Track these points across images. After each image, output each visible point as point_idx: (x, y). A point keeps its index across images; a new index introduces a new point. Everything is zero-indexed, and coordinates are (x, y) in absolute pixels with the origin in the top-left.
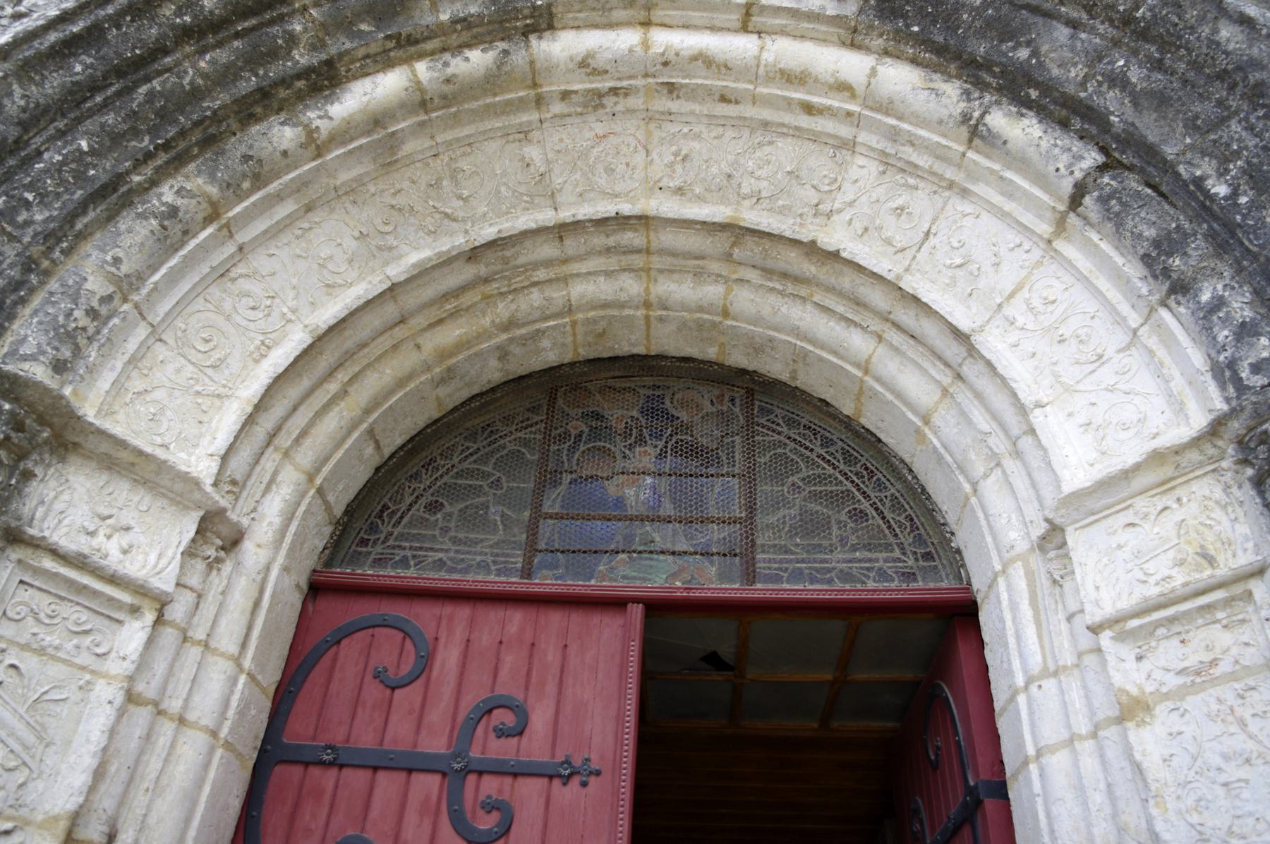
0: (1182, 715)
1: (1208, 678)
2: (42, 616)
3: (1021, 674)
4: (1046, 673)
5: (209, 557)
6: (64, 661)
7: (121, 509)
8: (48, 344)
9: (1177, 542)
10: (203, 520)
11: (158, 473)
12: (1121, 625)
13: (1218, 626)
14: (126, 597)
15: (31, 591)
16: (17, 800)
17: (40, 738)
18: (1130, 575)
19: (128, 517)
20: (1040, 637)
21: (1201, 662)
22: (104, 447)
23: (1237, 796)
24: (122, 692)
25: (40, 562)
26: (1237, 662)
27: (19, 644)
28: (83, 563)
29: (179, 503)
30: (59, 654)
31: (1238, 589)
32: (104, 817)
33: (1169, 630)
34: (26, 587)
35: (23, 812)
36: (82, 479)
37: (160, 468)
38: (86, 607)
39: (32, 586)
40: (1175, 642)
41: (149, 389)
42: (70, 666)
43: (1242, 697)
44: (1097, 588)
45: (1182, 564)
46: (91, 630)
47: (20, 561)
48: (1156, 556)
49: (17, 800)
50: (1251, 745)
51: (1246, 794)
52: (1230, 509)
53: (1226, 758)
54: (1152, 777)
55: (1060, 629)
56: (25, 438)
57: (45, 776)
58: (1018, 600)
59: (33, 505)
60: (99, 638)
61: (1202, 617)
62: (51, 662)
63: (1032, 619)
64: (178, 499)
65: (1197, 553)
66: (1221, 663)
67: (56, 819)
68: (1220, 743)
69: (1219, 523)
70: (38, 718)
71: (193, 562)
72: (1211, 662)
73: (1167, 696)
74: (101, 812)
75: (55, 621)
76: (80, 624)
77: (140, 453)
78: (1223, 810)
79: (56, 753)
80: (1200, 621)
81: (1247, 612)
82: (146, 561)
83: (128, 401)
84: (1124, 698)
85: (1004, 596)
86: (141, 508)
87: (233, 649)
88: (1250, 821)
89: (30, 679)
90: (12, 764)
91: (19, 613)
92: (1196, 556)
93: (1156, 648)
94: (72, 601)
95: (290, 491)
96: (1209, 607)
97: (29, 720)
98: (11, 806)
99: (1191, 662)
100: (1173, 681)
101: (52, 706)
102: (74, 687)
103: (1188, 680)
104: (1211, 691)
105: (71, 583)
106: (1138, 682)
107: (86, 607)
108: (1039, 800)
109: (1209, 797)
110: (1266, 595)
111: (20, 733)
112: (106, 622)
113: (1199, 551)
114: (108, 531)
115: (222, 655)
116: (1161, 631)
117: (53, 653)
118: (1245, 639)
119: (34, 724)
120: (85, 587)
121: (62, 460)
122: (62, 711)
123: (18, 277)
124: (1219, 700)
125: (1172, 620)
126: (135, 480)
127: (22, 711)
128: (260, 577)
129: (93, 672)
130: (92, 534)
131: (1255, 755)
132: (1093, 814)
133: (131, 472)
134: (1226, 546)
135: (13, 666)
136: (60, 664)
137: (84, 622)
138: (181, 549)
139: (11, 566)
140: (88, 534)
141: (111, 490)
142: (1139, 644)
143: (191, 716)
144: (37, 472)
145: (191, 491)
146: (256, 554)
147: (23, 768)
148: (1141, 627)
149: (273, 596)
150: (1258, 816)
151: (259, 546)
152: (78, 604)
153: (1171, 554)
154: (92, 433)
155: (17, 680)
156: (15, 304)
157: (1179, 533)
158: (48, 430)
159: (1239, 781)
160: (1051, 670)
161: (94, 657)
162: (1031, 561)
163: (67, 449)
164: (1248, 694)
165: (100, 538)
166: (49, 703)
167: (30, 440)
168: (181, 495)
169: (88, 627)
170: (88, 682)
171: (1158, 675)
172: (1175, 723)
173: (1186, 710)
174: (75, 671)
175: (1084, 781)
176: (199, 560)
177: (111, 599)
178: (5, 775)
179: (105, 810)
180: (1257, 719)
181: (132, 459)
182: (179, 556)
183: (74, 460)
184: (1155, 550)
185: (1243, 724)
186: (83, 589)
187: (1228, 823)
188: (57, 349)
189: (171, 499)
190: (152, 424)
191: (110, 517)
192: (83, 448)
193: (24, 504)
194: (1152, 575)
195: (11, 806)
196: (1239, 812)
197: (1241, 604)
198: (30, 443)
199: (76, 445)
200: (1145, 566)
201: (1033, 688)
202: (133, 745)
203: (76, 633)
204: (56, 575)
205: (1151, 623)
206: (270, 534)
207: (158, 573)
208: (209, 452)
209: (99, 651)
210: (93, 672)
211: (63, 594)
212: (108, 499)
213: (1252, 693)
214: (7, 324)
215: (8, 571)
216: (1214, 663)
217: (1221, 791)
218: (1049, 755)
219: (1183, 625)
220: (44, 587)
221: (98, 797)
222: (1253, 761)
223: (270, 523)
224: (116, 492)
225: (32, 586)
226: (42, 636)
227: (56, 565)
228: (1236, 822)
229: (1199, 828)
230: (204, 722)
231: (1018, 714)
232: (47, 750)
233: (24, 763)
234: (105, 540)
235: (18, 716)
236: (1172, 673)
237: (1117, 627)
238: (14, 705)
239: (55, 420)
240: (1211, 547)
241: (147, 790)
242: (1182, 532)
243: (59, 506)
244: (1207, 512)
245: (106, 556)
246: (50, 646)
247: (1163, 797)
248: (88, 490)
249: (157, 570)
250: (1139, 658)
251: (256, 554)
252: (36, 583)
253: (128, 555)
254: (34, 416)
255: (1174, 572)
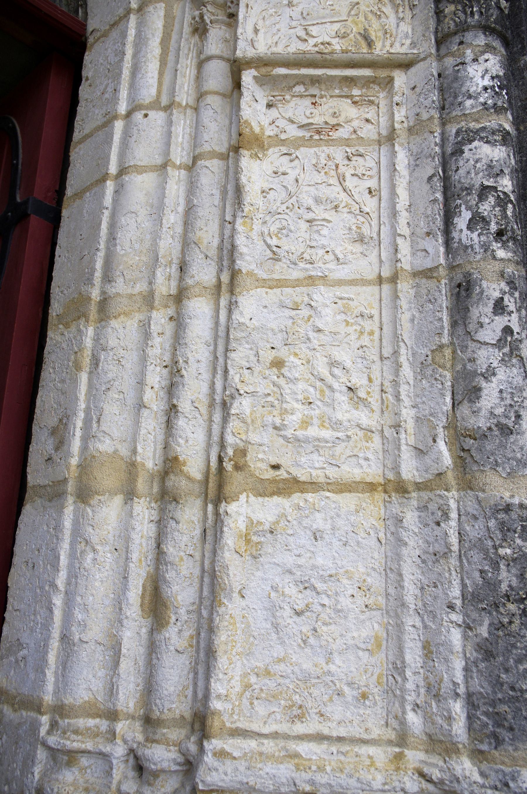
0: (291, 161)
1: (326, 138)
3: (125, 104)
4: (156, 105)
9: (345, 18)
12: (269, 69)
13: (349, 101)
18: (292, 31)
20: (161, 74)
21: (326, 123)
23: (318, 232)
26: (355, 132)
31: (383, 73)
33: (306, 90)
40: (307, 102)
43: (349, 159)
44: (256, 31)
45: (344, 37)
48: (322, 23)
50: (343, 196)
51: (325, 231)
52: (401, 9)
53: (318, 201)
54: (249, 201)
55: (185, 73)
58: (150, 36)
61: (341, 89)
63: (158, 57)
65: (360, 33)
66: (341, 130)
68: (317, 189)
69: (387, 17)
72: (334, 126)
73: (283, 142)
78: (301, 240)
80: (337, 91)
81: (378, 97)
84: (247, 130)
85: (132, 32)
88: (321, 252)
92: (358, 37)
93: (289, 102)
96: (350, 81)
99: (318, 120)
100: (293, 132)
103: (308, 135)
104: (325, 148)
106: (262, 124)
108: (106, 213)
109: (292, 228)
110: (404, 86)
113: (362, 32)
116: (299, 89)
118: (368, 116)
124: (328, 156)
125: (315, 81)
131: (343, 204)
132: (164, 229)
134: (388, 36)
142: (274, 94)
148: (286, 76)
150: (327, 249)
153: (336, 26)
157: (350, 12)
159: (324, 220)
160: (162, 105)
162: (175, 7)
164: (354, 158)
171: (282, 123)
172: (284, 164)
173: (297, 157)
175: (166, 200)
180: (356, 178)
184: (324, 18)
185: (342, 179)
187: (302, 250)
194: (314, 37)
196: (313, 244)
197: (377, 88)
200: (310, 28)
201: (138, 116)
205: (296, 76)
213: (360, 159)
216: (335, 127)
217: (304, 226)
218: (135, 174)
219: (321, 90)
222: (340, 209)
228: (309, 250)
229: (275, 249)
231: (112, 135)
236: (295, 126)
237: (264, 70)
240: (373, 34)
242: (353, 13)
244: (380, 6)
247: (252, 219)
250: (269, 106)
255: (334, 41)
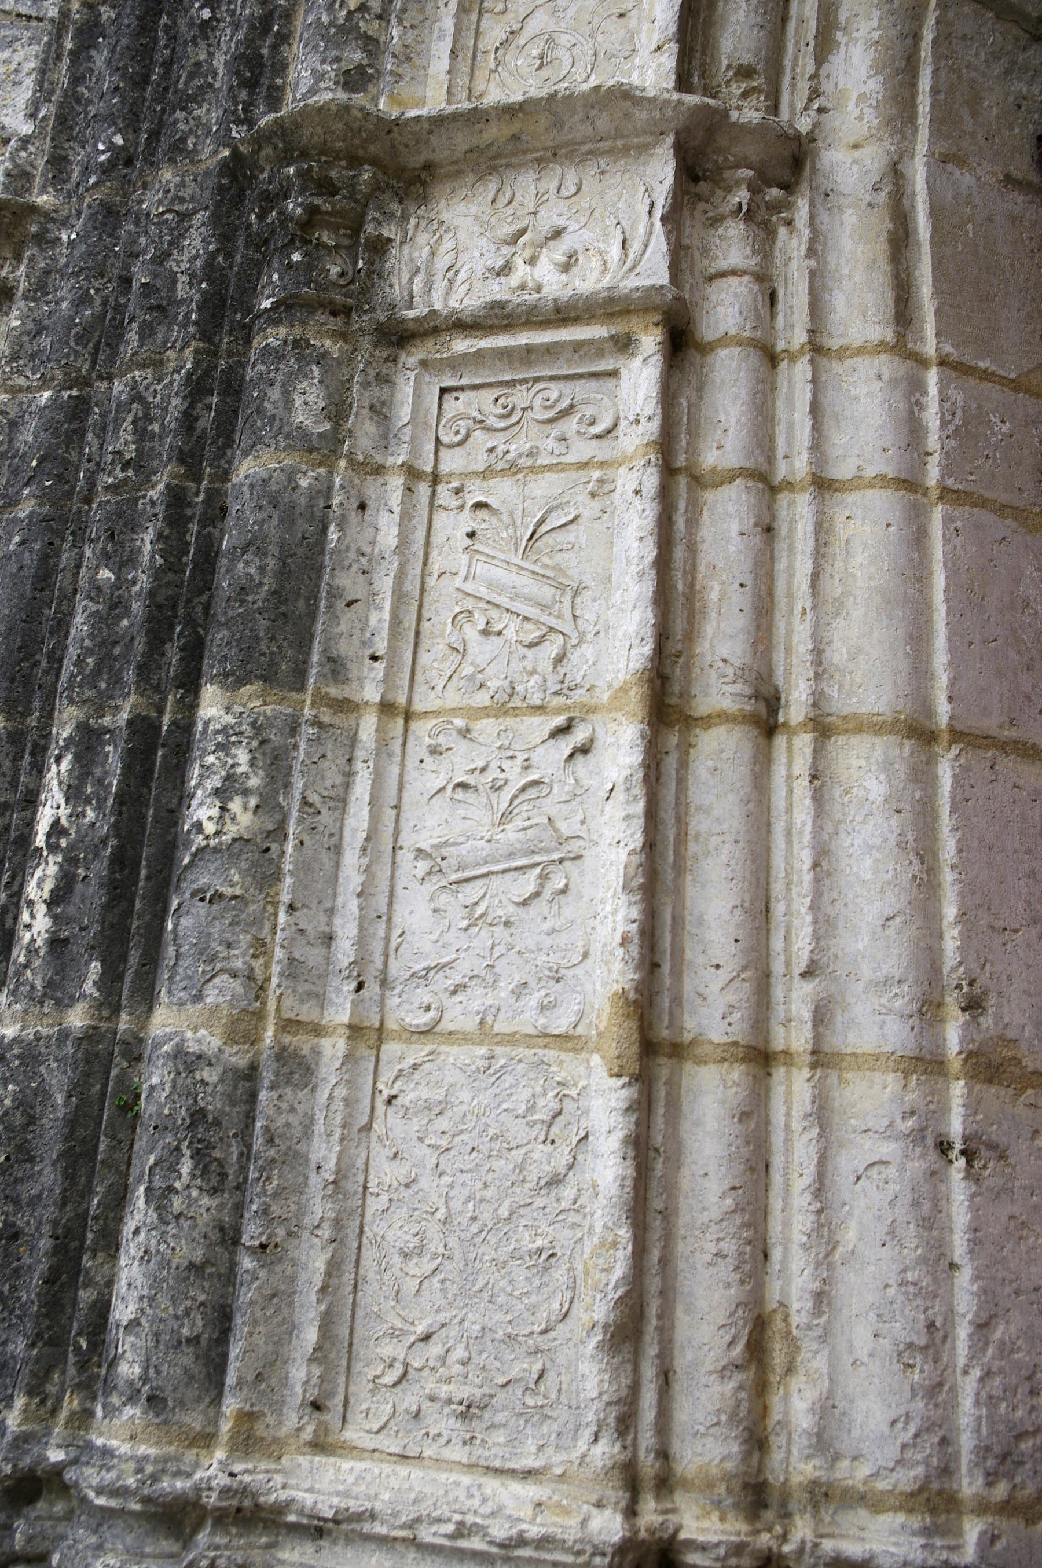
2: (492, 421)
5: (740, 204)
6: (551, 468)
7: (535, 213)
8: (323, 62)
10: (679, 149)
11: (558, 124)
14: (596, 331)
15: (462, 396)
16: (562, 682)
17: (561, 587)
19: (549, 218)
22: (462, 141)
24: (652, 470)
25: (449, 350)
27: (477, 474)
28: (508, 316)
29: (626, 150)
30: (539, 462)
32: (730, 671)
34: (455, 394)
35: (578, 695)
36: (461, 208)
37: (554, 114)
38: (552, 378)
39: (462, 389)
41: (516, 27)
42: (563, 470)
46: (572, 406)
47: (424, 364)
49: (562, 682)
56: (344, 197)
57: (590, 637)
59: (405, 280)
60: (589, 411)
62: (531, 477)
64: (620, 143)
67: (623, 689)
70: (546, 560)
71: (720, 231)
74: (721, 664)
75: (514, 419)
76: (551, 407)
77: (510, 111)
79: (594, 600)
82: (605, 262)
83: (493, 66)
86: (567, 194)
87: (881, 331)
89: (511, 514)
90: (534, 635)
91: (457, 433)
94: (525, 381)
95: (875, 23)
97: (532, 567)
98: (556, 693)
101: (559, 537)
102: (583, 497)
105: (505, 355)
107: (552, 378)
111: (526, 591)
112: (593, 384)
114: (527, 254)
115: (860, 351)
117: (529, 463)
119: (541, 571)
120: (529, 349)
121: (424, 199)
122: (577, 537)
123: (258, 11)
126: (539, 161)
127: (517, 560)
128: (882, 197)
129: (602, 464)
130: (505, 270)
133: (525, 152)
135: (479, 505)
136: (547, 475)
137: (558, 400)
138: (658, 213)
139: (412, 375)
140: (498, 275)
141: (508, 195)
143: (842, 471)
144: (386, 233)
145: (628, 116)
146: (855, 162)
147: (553, 636)
149: (935, 213)
151: (856, 146)
152: (537, 380)
154: (430, 132)
155: (494, 521)
156: (275, 48)
158: (366, 167)
161: (594, 442)
163: (424, 184)
165: (521, 271)
166: (554, 535)
167: (352, 197)
168: (618, 134)
169: (565, 403)
170: (601, 481)
174: (573, 474)
176: (729, 223)
177: (577, 346)
178: (530, 653)
179: (724, 661)
181: (507, 131)
182: (658, 224)
183: (440, 190)
186: (529, 354)
188: (338, 59)
189: (610, 152)
190: (545, 73)
191: (522, 232)
192: (441, 167)
193: (391, 286)
195: (556, 693)
198: (356, 201)
199: (428, 166)
202: (732, 549)
203: (550, 421)
204: (480, 354)
206: (869, 114)
207: (634, 267)
208: (654, 47)
209: (597, 429)
210: (602, 464)
211: (508, 378)
212: (510, 211)
214: (279, 81)
215: (412, 384)
220: (477, 381)
221: (707, 645)
223: (862, 97)
224: (518, 195)
225: (462, 389)
226: (502, 448)
227: (474, 342)
230: (870, 472)
232: (578, 600)
233: (551, 629)
234: (528, 268)
235: (514, 569)
238: (502, 556)
239: (372, 149)
241: (804, 612)
243: (442, 262)
245: (538, 289)
246: (520, 455)
248: (476, 218)
249: (628, 265)
251: (855, 162)
252: (464, 382)
253: (575, 270)
254: (343, 163)
